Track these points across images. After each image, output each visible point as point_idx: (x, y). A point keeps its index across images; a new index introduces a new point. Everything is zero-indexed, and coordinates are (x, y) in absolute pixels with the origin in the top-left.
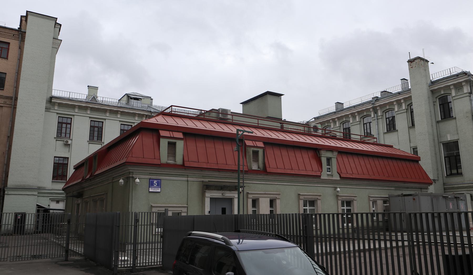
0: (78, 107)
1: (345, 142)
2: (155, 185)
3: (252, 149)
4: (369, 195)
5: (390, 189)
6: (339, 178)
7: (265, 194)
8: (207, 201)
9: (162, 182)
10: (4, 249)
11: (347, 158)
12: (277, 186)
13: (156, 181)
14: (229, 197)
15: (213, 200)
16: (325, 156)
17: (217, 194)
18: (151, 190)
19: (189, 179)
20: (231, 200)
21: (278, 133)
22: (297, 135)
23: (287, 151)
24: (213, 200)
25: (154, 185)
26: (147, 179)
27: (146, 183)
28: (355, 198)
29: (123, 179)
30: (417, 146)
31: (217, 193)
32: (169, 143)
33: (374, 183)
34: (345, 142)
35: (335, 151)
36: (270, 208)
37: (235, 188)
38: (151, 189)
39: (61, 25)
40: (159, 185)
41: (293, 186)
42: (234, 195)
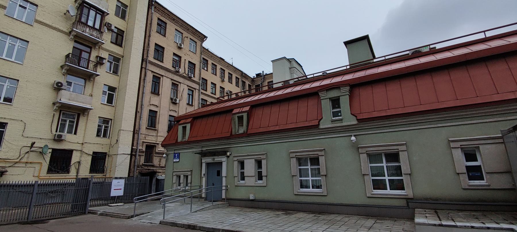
1: (467, 47)
3: (237, 115)
4: (450, 139)
5: (366, 133)
6: (355, 122)
7: (248, 155)
8: (204, 165)
10: (39, 195)
11: (486, 68)
12: (265, 145)
14: (218, 161)
15: (208, 165)
16: (326, 97)
17: (209, 160)
18: (174, 161)
19: (203, 149)
20: (221, 163)
21: (467, 49)
22: (466, 49)
23: (507, 63)
24: (208, 165)
26: (343, 138)
27: (172, 156)
29: (165, 154)
30: (75, 133)
33: (382, 123)
34: (487, 44)
36: (386, 164)
37: (223, 153)
40: (179, 157)
42: (224, 159)
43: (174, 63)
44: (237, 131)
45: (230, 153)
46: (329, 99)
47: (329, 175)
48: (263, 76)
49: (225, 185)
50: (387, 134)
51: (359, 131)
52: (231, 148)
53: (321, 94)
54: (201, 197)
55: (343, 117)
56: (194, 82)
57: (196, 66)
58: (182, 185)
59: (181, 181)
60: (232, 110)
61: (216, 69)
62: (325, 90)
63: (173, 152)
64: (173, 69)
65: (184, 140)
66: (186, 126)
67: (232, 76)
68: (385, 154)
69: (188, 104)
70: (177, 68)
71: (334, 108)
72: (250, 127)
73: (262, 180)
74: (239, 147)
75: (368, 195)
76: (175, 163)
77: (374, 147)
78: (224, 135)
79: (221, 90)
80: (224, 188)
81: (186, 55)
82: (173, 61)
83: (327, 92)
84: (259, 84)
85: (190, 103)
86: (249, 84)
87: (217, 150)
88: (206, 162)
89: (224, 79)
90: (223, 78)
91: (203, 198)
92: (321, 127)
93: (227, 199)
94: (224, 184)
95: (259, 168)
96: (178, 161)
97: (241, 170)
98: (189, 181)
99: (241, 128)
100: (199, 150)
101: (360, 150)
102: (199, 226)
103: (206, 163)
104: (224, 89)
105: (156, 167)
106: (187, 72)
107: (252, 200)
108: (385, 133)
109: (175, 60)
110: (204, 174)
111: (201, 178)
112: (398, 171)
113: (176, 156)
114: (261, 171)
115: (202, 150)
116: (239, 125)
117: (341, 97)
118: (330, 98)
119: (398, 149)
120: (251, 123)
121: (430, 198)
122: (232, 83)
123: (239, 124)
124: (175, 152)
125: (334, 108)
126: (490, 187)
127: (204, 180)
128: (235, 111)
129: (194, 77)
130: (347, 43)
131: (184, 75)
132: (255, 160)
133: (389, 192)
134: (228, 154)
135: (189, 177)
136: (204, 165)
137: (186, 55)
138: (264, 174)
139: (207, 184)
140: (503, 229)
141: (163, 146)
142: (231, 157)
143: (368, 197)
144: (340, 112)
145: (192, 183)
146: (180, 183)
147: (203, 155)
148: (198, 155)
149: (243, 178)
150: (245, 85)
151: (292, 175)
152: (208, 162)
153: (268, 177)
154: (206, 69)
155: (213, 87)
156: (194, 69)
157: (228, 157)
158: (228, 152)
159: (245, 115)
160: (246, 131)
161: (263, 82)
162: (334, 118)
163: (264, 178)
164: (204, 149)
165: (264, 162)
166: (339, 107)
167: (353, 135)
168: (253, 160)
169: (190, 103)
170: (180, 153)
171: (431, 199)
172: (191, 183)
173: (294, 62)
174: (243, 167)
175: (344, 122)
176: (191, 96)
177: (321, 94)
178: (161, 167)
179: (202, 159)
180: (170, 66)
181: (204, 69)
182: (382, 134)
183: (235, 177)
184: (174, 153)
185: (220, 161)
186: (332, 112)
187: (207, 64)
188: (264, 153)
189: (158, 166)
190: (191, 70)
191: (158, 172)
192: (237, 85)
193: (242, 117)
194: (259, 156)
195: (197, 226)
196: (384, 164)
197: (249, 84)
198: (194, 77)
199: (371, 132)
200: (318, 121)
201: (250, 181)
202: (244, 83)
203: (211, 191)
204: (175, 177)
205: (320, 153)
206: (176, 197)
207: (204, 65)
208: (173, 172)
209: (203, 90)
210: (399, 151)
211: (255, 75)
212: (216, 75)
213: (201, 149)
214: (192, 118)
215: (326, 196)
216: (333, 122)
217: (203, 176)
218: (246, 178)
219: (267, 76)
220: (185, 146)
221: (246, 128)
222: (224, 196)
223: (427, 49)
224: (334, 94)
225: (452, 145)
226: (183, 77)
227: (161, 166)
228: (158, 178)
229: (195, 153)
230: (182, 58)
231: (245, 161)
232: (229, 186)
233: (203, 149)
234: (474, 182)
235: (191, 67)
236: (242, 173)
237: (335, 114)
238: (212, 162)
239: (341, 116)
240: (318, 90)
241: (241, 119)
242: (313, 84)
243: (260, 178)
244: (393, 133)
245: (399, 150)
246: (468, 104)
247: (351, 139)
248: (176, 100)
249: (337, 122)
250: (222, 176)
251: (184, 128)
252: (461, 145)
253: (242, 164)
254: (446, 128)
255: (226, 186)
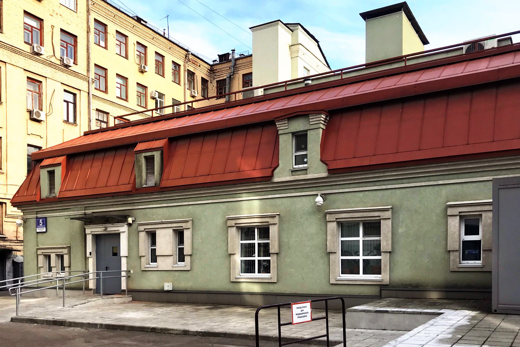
0: (287, 120)
2: (41, 224)
3: (144, 154)
5: (341, 191)
7: (162, 223)
8: (89, 238)
9: (49, 220)
12: (190, 207)
13: (42, 220)
14: (113, 232)
15: (97, 238)
16: (286, 131)
17: (99, 230)
18: (38, 231)
19: (86, 211)
24: (97, 238)
25: (40, 224)
26: (308, 198)
28: (184, 225)
31: (97, 227)
32: (49, 172)
35: (311, 112)
37: (122, 218)
38: (38, 229)
39: (405, 3)
41: (220, 204)
42: (123, 229)
43: (28, 34)
44: (143, 181)
45: (134, 219)
46: (291, 134)
47: (283, 254)
48: (233, 61)
49: (126, 270)
50: (370, 193)
51: (332, 187)
52: (136, 211)
53: (280, 126)
54: (87, 289)
55: (309, 164)
56: (76, 74)
57: (78, 40)
58: (54, 270)
59: (52, 264)
60: (134, 145)
61: (126, 44)
62: (286, 119)
63: (33, 216)
64: (27, 48)
65: (53, 195)
66: (54, 170)
67: (163, 60)
68: (363, 223)
69: (67, 121)
70: (35, 45)
71: (298, 149)
72: (165, 176)
73: (184, 261)
74: (148, 210)
75: (332, 281)
76: (39, 235)
77: (348, 212)
78: (123, 188)
79: (141, 90)
80: (123, 274)
81: (55, 15)
82: (25, 29)
83: (290, 122)
84: (225, 77)
85: (71, 120)
86: (202, 78)
87: (108, 213)
88: (93, 233)
89: (144, 67)
90: (143, 65)
91: (91, 290)
92: (276, 179)
93: (128, 291)
94: (124, 267)
95: (153, 245)
96: (45, 230)
97: (151, 246)
98: (66, 264)
99: (150, 177)
100: (80, 213)
101: (328, 216)
102: (68, 322)
103: (93, 235)
104: (145, 87)
105: (11, 241)
106: (58, 55)
107: (168, 292)
108: (366, 192)
109: (30, 27)
110: (90, 253)
111: (86, 259)
112: (376, 249)
113: (40, 222)
114: (155, 249)
115: (85, 214)
116: (148, 171)
117: (309, 133)
118: (293, 134)
119: (380, 216)
120: (166, 171)
121: (409, 284)
122: (163, 76)
123: (147, 169)
124: (39, 216)
125: (298, 149)
126: (484, 270)
127: (91, 263)
128: (140, 147)
129: (75, 63)
130: (367, 16)
131: (53, 60)
132: (173, 229)
133: (361, 277)
134: (130, 220)
135: (66, 258)
136: (89, 238)
137: (55, 15)
138: (187, 250)
139: (98, 267)
140: (435, 314)
141: (14, 204)
142: (134, 226)
143: (331, 284)
144: (306, 156)
145: (71, 266)
146: (52, 267)
147: (87, 222)
148: (78, 223)
149: (154, 259)
150: (194, 80)
151: (229, 253)
152: (96, 233)
153: (193, 257)
154: (102, 44)
155: (121, 85)
156: (75, 46)
157: (130, 225)
158: (129, 216)
159: (157, 155)
160: (158, 182)
161: (232, 74)
162: (297, 166)
163: (187, 259)
164: (89, 212)
165: (187, 234)
166: (306, 149)
167: (319, 194)
168: (171, 231)
169: (71, 120)
170: (47, 218)
171: (410, 285)
172: (69, 267)
173: (300, 31)
174: (154, 243)
175: (310, 173)
176: (71, 106)
177: (280, 126)
178: (19, 241)
179: (85, 229)
180: (20, 44)
181: (99, 45)
182: (363, 193)
183: (141, 256)
184: (37, 218)
185: (116, 232)
186: (295, 156)
187: (106, 32)
188: (276, 214)
189: (15, 239)
190: (69, 48)
191: (15, 250)
192: (177, 80)
193: (152, 157)
194: (179, 225)
195: (65, 322)
196: (361, 238)
197: (202, 78)
198: (75, 63)
199: (347, 190)
200: (271, 170)
201: (163, 264)
202: (191, 74)
203: (100, 278)
204: (41, 258)
205: (184, 225)
206: (48, 289)
207: (99, 35)
208: (38, 249)
209: (99, 90)
210: (380, 220)
211: (218, 57)
212: (126, 57)
213: (83, 212)
214: (64, 155)
215: (276, 282)
216: (294, 173)
217: (88, 255)
218: (159, 259)
219: (240, 61)
220: (59, 206)
221: (158, 178)
222: (124, 287)
223: (492, 44)
224: (298, 126)
225: (450, 211)
226: (51, 65)
227: (19, 239)
228: (15, 260)
229: (72, 219)
230: (45, 23)
231: (158, 232)
232: (132, 272)
233: (86, 211)
234: (468, 263)
235: (67, 43)
236: (153, 251)
237: (300, 160)
238: (104, 233)
239: (306, 163)
240: (275, 118)
241: (150, 160)
242: (276, 104)
243: (181, 258)
244: (378, 192)
245: (381, 218)
246: (510, 149)
247: (316, 201)
248: (38, 114)
249: (299, 173)
250: (121, 256)
251: (51, 174)
252: (460, 212)
253: (152, 236)
254: (448, 186)
255: (128, 272)
